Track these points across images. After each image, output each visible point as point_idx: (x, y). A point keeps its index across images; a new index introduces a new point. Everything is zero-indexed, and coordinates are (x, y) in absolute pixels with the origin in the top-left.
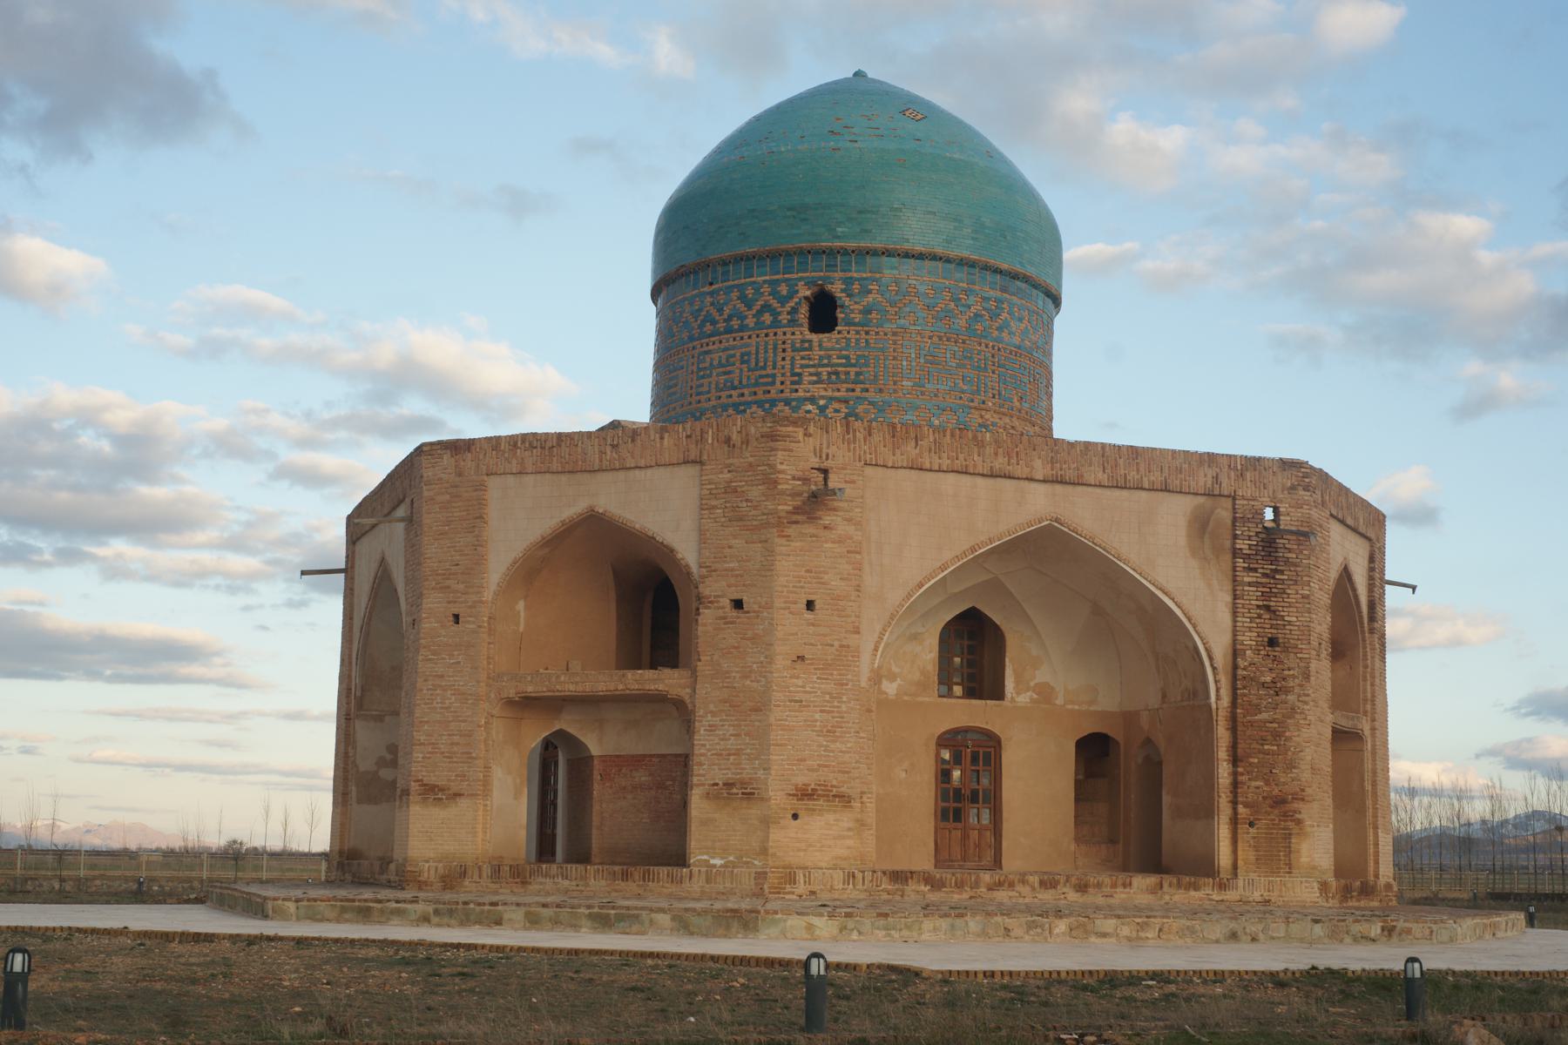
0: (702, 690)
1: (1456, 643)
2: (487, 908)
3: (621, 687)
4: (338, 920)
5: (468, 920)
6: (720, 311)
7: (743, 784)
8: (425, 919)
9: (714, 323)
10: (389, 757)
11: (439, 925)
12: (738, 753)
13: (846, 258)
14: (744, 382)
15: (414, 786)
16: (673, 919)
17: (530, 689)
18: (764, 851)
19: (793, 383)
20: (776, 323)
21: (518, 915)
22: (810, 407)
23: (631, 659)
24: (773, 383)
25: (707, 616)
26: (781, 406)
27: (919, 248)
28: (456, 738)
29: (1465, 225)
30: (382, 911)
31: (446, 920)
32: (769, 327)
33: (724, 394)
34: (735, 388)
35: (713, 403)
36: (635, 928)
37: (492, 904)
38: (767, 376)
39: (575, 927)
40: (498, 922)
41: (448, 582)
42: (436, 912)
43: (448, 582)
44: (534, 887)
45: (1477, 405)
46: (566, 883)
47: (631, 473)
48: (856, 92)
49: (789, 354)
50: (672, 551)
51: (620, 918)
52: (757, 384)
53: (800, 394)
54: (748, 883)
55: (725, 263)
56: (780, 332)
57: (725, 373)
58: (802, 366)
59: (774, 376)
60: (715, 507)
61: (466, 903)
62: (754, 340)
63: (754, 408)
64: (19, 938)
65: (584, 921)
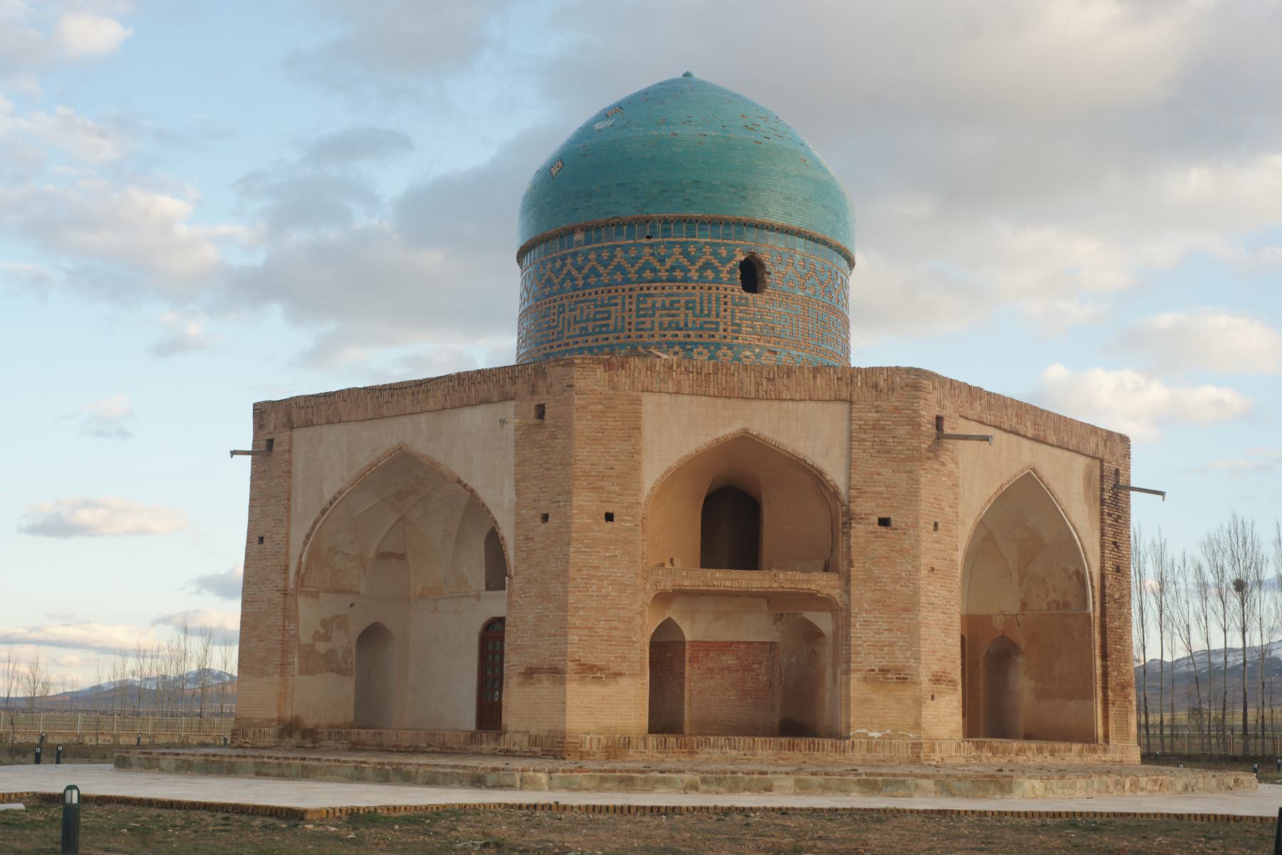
0: (855, 591)
1: (142, 531)
2: (756, 776)
3: (775, 585)
4: (598, 790)
5: (737, 786)
6: (662, 261)
7: (898, 670)
8: (694, 787)
9: (654, 270)
10: (322, 631)
11: (707, 792)
12: (891, 645)
13: (666, 226)
14: (690, 325)
15: (571, 666)
16: (936, 784)
17: (687, 583)
18: (917, 726)
19: (733, 331)
20: (717, 279)
21: (789, 782)
22: (748, 353)
23: (709, 558)
24: (717, 329)
25: (858, 530)
26: (724, 350)
27: (819, 234)
28: (615, 624)
29: (169, 204)
30: (646, 781)
31: (714, 788)
32: (712, 282)
33: (669, 333)
34: (681, 329)
35: (657, 339)
36: (901, 792)
37: (761, 773)
38: (712, 323)
39: (846, 792)
40: (769, 789)
41: (600, 484)
42: (704, 781)
43: (600, 484)
44: (701, 757)
45: (170, 347)
46: (734, 752)
47: (784, 404)
48: (676, 93)
49: (729, 307)
50: (821, 473)
51: (887, 784)
52: (701, 328)
53: (740, 341)
54: (905, 753)
55: (666, 221)
56: (722, 287)
57: (670, 315)
58: (741, 319)
59: (717, 323)
60: (864, 440)
61: (733, 772)
62: (698, 290)
63: (701, 349)
64: (6, 812)
65: (853, 787)
